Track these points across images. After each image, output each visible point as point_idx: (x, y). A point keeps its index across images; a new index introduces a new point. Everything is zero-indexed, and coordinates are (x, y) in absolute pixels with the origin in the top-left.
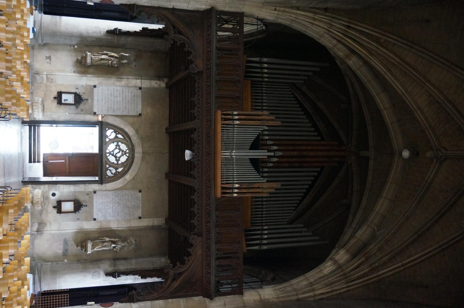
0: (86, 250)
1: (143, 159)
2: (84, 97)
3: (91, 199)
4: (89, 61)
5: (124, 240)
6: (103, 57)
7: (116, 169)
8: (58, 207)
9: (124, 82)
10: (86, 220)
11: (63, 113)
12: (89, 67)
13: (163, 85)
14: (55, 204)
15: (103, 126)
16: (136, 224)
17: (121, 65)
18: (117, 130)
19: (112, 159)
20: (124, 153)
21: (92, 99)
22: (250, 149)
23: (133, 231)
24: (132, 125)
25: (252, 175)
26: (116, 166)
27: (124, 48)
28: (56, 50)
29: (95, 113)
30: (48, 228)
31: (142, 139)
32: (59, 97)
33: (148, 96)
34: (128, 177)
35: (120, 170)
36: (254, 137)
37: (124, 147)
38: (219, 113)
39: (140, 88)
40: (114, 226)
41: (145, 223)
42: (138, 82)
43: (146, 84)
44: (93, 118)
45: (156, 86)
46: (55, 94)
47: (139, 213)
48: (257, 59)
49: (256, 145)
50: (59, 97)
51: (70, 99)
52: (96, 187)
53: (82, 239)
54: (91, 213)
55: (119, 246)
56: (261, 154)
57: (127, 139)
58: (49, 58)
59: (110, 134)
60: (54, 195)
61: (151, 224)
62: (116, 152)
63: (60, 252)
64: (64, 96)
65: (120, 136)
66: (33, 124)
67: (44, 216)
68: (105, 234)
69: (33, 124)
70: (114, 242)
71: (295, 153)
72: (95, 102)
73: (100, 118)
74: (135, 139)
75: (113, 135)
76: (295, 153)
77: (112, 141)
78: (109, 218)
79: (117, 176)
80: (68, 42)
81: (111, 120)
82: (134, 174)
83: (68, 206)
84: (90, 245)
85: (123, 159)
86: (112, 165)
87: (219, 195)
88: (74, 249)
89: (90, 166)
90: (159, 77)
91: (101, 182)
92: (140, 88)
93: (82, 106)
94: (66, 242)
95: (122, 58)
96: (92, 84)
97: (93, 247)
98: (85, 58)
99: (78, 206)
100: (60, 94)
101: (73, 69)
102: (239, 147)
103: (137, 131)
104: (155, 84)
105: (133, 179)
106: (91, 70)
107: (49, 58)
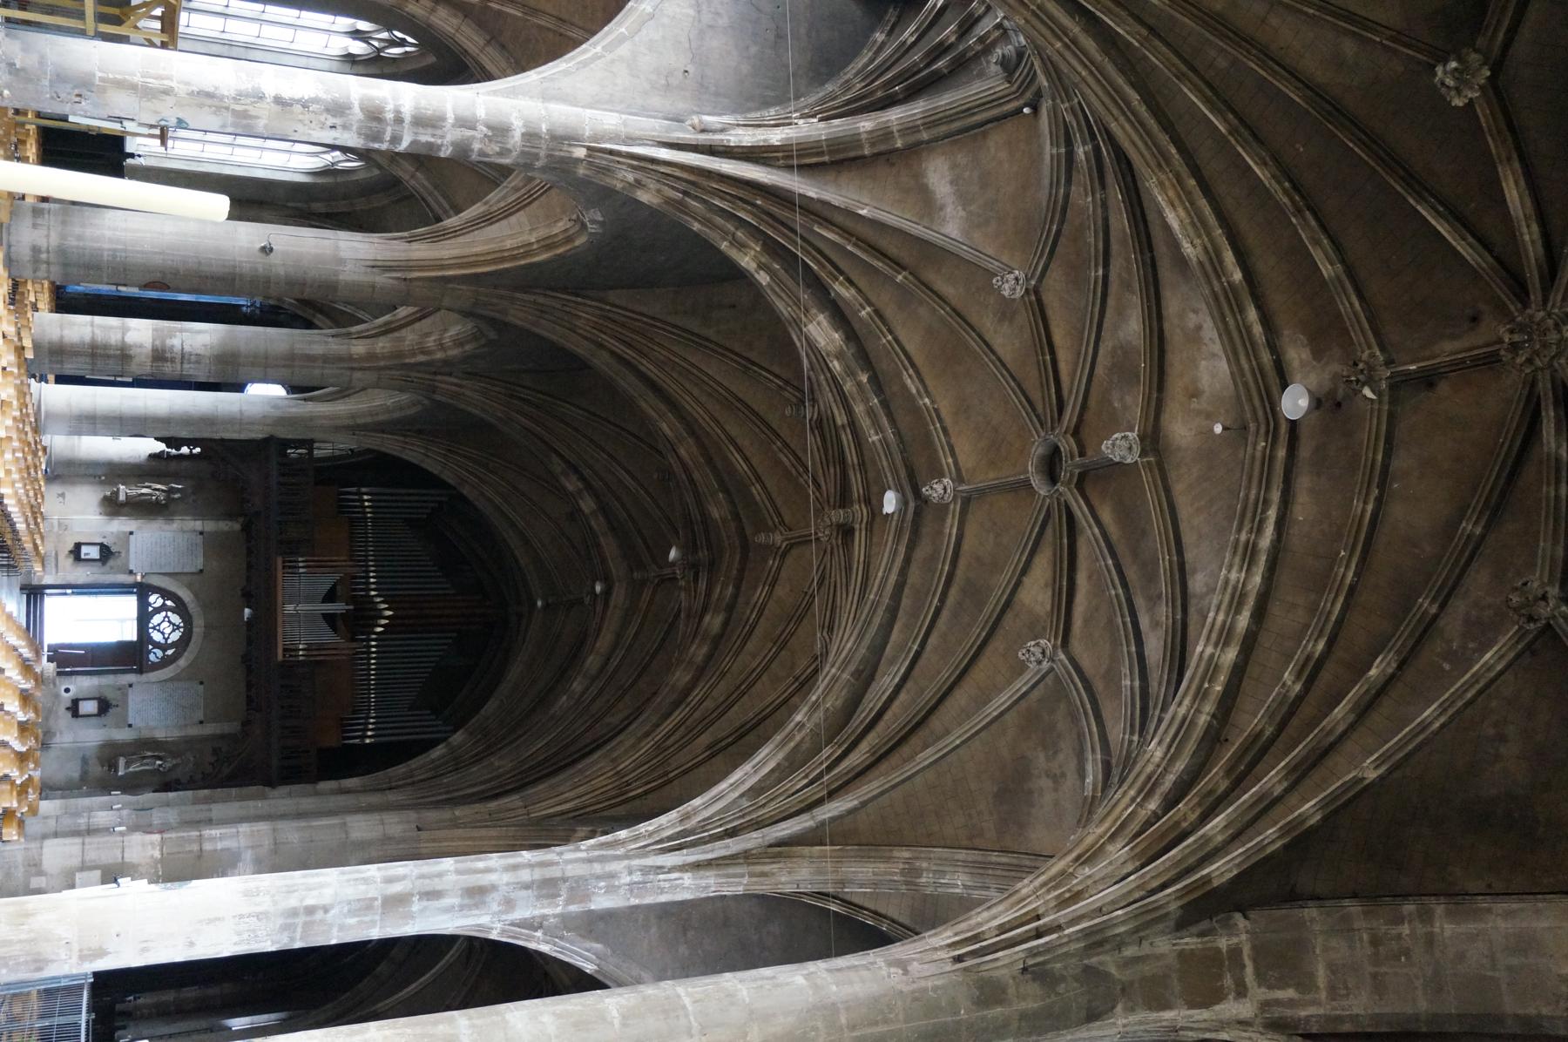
0: (116, 771)
1: (206, 636)
2: (114, 549)
3: (125, 695)
4: (122, 497)
5: (174, 755)
6: (144, 491)
7: (164, 650)
8: (74, 709)
9: (176, 525)
10: (118, 726)
11: (82, 575)
12: (123, 505)
13: (237, 527)
14: (69, 704)
15: (142, 591)
16: (194, 731)
17: (169, 500)
18: (165, 594)
19: (157, 637)
20: (176, 627)
21: (128, 551)
22: (323, 602)
23: (189, 742)
24: (189, 586)
25: (328, 637)
26: (163, 647)
27: (176, 477)
28: (73, 483)
29: (131, 572)
30: (57, 739)
31: (205, 607)
32: (76, 551)
33: (211, 543)
34: (182, 662)
35: (170, 652)
36: (328, 587)
37: (176, 619)
38: (279, 560)
39: (201, 533)
40: (160, 735)
41: (209, 729)
42: (198, 525)
43: (210, 526)
44: (128, 579)
45: (226, 529)
46: (71, 546)
47: (200, 715)
48: (354, 489)
49: (330, 597)
50: (76, 551)
51: (94, 553)
52: (131, 678)
53: (110, 754)
54: (125, 717)
55: (168, 765)
56: (338, 607)
57: (181, 608)
58: (62, 495)
59: (155, 600)
60: (67, 690)
61: (218, 732)
62: (166, 628)
63: (76, 775)
64: (84, 549)
65: (169, 603)
66: (34, 594)
67: (51, 722)
68: (143, 746)
69: (34, 594)
70: (159, 758)
71: (412, 612)
72: (132, 556)
73: (139, 578)
74: (192, 607)
75: (160, 602)
76: (412, 612)
77: (157, 611)
78: (152, 724)
79: (165, 662)
80: (91, 471)
81: (156, 581)
82: (192, 657)
83: (89, 707)
84: (122, 761)
85: (176, 636)
86: (157, 645)
87: (280, 657)
88: (96, 770)
89: (129, 657)
90: (229, 516)
91: (140, 671)
92: (201, 533)
93: (111, 563)
94: (85, 761)
95: (171, 491)
96: (129, 529)
97: (128, 765)
98: (117, 493)
99: (104, 706)
100: (78, 546)
101: (98, 510)
102: (309, 599)
103: (196, 595)
104: (224, 526)
105: (190, 665)
106: (126, 509)
107: (62, 495)
